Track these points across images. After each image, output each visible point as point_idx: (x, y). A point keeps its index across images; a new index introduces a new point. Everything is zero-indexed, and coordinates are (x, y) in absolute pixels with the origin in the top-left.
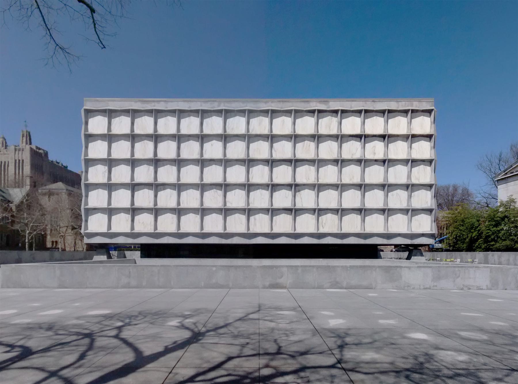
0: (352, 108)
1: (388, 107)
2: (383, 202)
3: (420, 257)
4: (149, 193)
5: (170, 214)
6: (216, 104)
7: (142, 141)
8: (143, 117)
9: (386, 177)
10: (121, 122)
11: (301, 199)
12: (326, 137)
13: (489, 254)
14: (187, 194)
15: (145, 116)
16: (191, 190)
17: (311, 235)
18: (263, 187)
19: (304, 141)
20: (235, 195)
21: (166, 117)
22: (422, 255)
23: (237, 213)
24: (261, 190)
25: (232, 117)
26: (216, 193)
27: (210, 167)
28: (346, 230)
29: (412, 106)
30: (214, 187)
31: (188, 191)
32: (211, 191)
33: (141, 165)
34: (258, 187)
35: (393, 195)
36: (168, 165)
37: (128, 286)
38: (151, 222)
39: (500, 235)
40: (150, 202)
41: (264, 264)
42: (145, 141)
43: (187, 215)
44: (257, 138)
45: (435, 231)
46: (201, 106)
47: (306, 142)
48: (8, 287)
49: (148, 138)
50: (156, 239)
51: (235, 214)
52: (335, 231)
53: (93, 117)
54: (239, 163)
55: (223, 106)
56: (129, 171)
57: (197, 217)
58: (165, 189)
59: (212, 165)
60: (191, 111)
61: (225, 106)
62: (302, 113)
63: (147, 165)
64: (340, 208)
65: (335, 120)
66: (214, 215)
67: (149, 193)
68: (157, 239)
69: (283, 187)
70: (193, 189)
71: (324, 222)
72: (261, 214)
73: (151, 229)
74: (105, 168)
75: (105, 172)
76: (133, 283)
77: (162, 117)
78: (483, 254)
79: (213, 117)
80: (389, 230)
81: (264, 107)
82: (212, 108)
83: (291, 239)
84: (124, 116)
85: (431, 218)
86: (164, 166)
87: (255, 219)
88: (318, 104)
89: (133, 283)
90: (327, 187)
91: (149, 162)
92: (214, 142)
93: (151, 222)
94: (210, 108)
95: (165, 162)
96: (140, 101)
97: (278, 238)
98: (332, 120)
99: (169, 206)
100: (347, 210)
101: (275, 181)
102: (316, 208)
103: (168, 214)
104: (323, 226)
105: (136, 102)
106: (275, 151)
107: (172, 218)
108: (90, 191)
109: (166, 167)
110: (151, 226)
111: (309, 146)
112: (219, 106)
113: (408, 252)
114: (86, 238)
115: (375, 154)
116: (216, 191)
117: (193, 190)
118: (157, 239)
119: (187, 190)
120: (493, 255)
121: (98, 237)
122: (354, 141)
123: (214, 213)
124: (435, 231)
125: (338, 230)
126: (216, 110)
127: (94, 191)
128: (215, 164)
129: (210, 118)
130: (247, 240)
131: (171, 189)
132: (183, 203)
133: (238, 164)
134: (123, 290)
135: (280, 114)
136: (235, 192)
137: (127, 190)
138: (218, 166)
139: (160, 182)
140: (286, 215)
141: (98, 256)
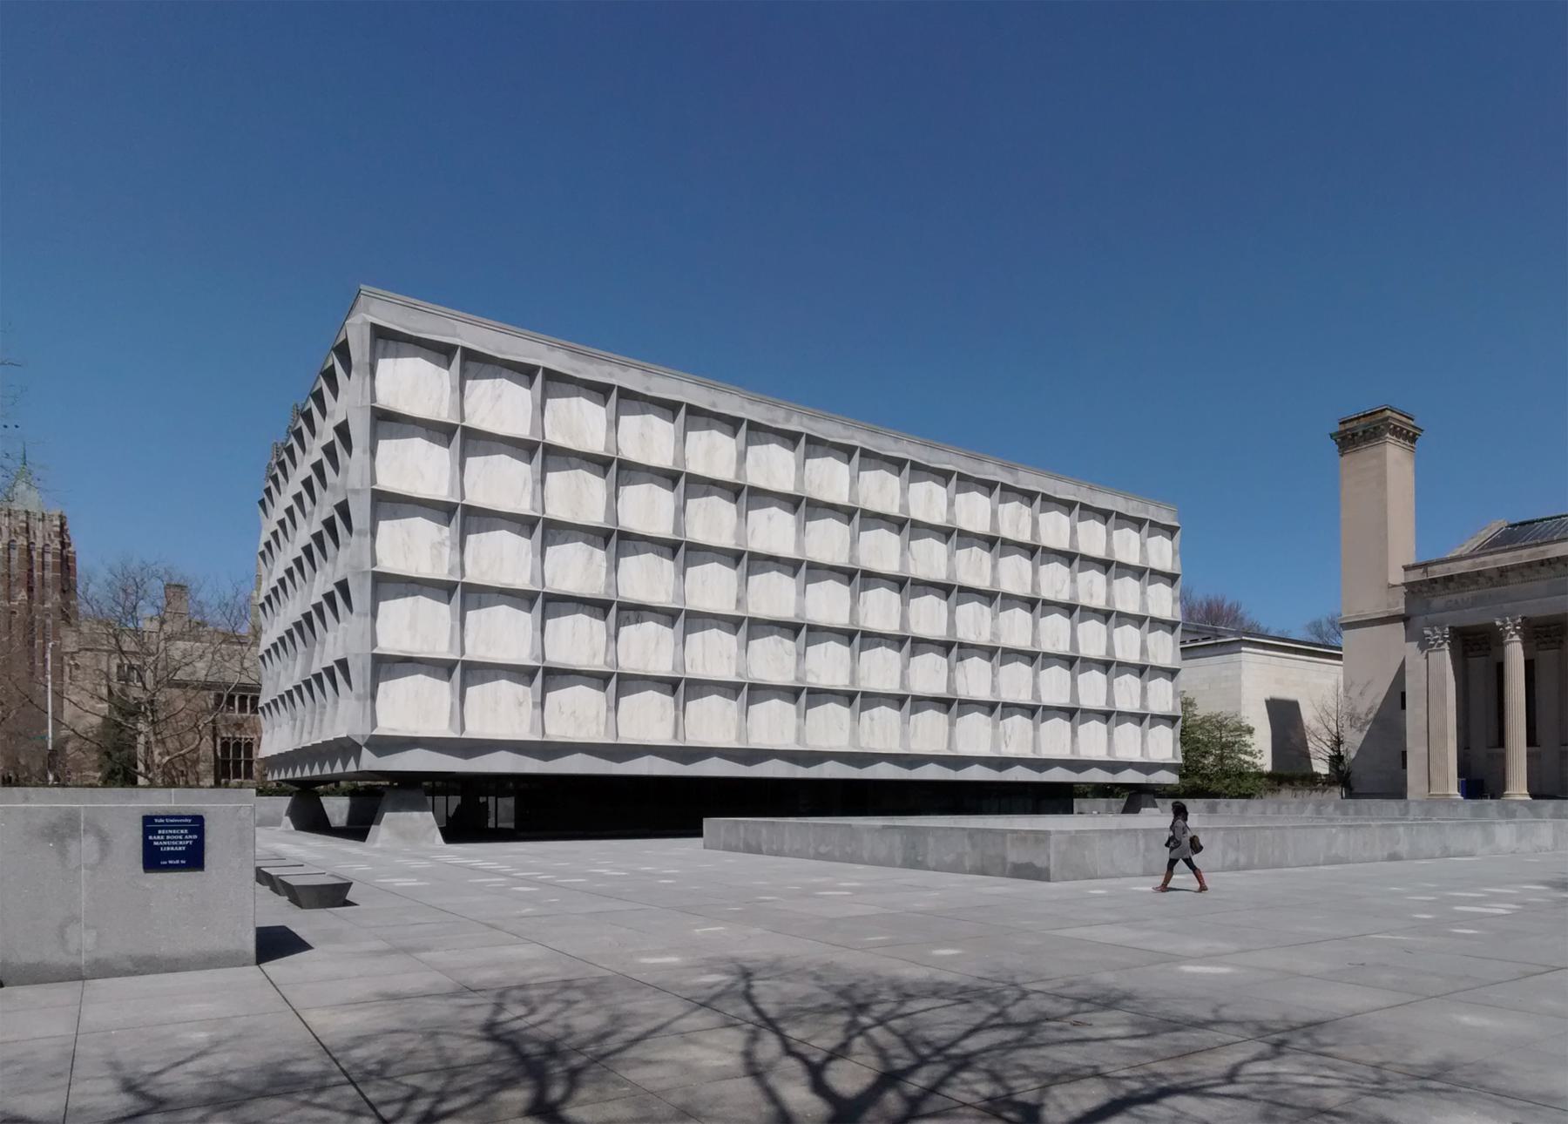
0: (1017, 484)
1: (862, 442)
2: (1105, 698)
3: (1153, 809)
4: (591, 627)
5: (656, 694)
6: (943, 456)
7: (571, 469)
8: (574, 400)
9: (1110, 647)
10: (500, 396)
11: (966, 677)
12: (826, 508)
13: (1217, 804)
14: (704, 643)
15: (578, 396)
16: (715, 630)
17: (987, 762)
18: (889, 642)
19: (972, 546)
20: (825, 656)
21: (644, 413)
22: (1156, 806)
23: (830, 702)
24: (884, 648)
25: (818, 457)
26: (780, 645)
27: (764, 575)
28: (558, 731)
29: (1147, 512)
30: (776, 629)
31: (706, 632)
32: (766, 639)
33: (566, 541)
34: (877, 640)
35: (1120, 684)
36: (651, 555)
37: (1393, 857)
38: (598, 713)
39: (171, 731)
40: (594, 656)
41: (1016, 827)
42: (580, 471)
43: (705, 699)
44: (876, 520)
45: (1180, 761)
46: (742, 408)
47: (975, 548)
48: (1065, 879)
49: (590, 464)
50: (614, 764)
51: (826, 703)
52: (941, 749)
53: (397, 356)
54: (836, 574)
55: (859, 439)
56: (527, 554)
57: (730, 704)
58: (642, 622)
59: (769, 571)
60: (720, 417)
61: (801, 425)
62: (968, 483)
63: (584, 542)
64: (613, 671)
65: (1027, 512)
66: (775, 703)
67: (591, 627)
68: (1041, 771)
69: (931, 646)
70: (719, 628)
71: (1009, 731)
72: (883, 708)
73: (598, 732)
74: (440, 530)
75: (439, 543)
76: (1243, 860)
77: (634, 413)
78: (1205, 803)
79: (770, 445)
80: (751, 741)
81: (893, 451)
82: (769, 420)
83: (946, 769)
84: (509, 379)
85: (1174, 734)
86: (637, 553)
87: (872, 719)
88: (999, 471)
89: (1243, 860)
90: (1013, 655)
91: (592, 537)
92: (774, 510)
93: (598, 713)
94: (763, 419)
95: (710, 554)
96: (563, 347)
97: (561, 757)
98: (1022, 511)
99: (655, 672)
100: (966, 704)
101: (915, 631)
102: (458, 658)
103: (651, 691)
104: (1006, 742)
105: (552, 347)
106: (914, 559)
107: (663, 704)
108: (385, 600)
109: (642, 557)
110: (598, 724)
111: (981, 560)
112: (788, 420)
113: (321, 798)
114: (369, 752)
115: (1091, 596)
116: (782, 643)
117: (719, 631)
118: (686, 764)
119: (703, 629)
120: (1228, 806)
121: (418, 750)
122: (1059, 564)
123: (775, 698)
124: (1180, 761)
125: (532, 730)
126: (426, 339)
127: (400, 602)
128: (779, 571)
129: (765, 447)
130: (1074, 774)
131: (658, 623)
132: (692, 666)
133: (834, 579)
134: (1326, 868)
135: (925, 474)
136: (826, 648)
137: (519, 609)
138: (786, 577)
139: (624, 598)
140: (936, 712)
141: (402, 814)
